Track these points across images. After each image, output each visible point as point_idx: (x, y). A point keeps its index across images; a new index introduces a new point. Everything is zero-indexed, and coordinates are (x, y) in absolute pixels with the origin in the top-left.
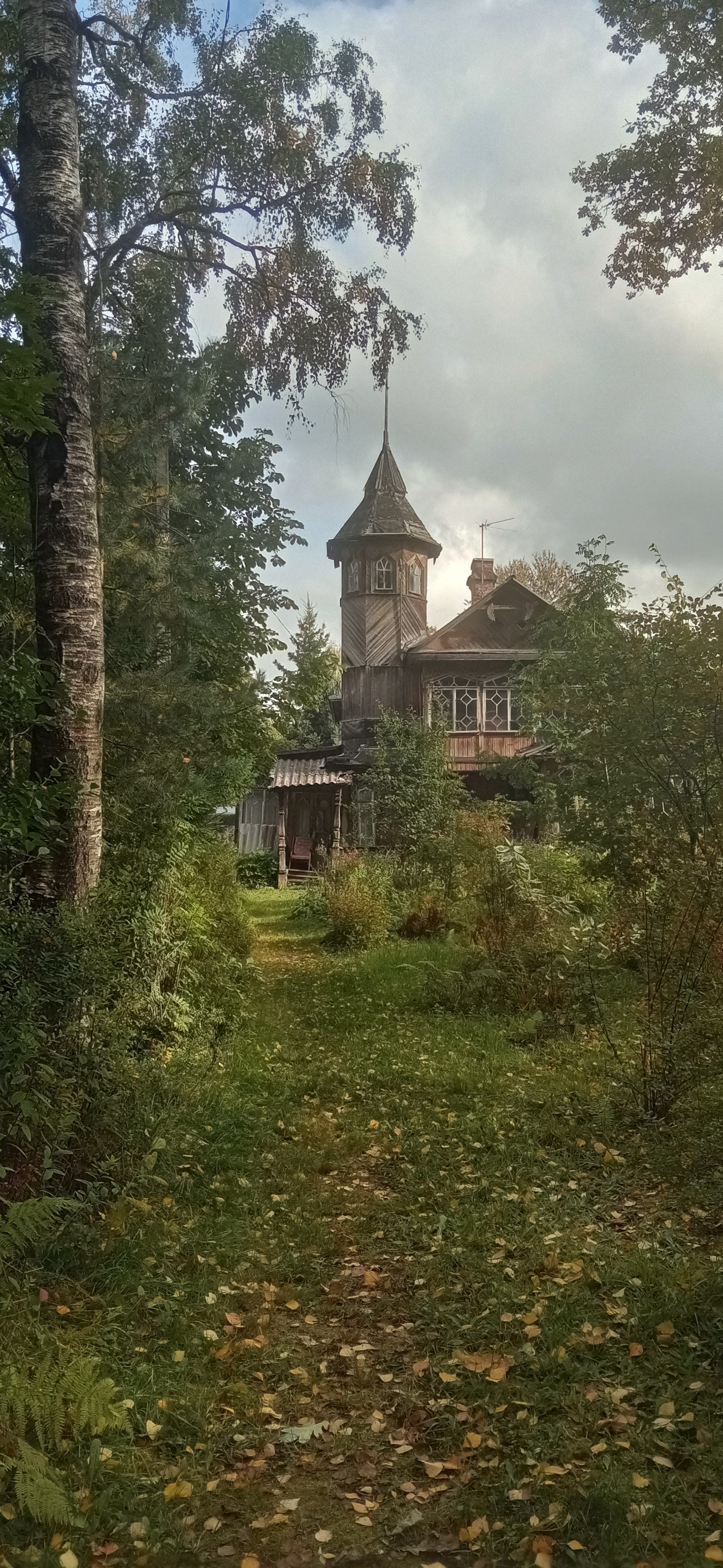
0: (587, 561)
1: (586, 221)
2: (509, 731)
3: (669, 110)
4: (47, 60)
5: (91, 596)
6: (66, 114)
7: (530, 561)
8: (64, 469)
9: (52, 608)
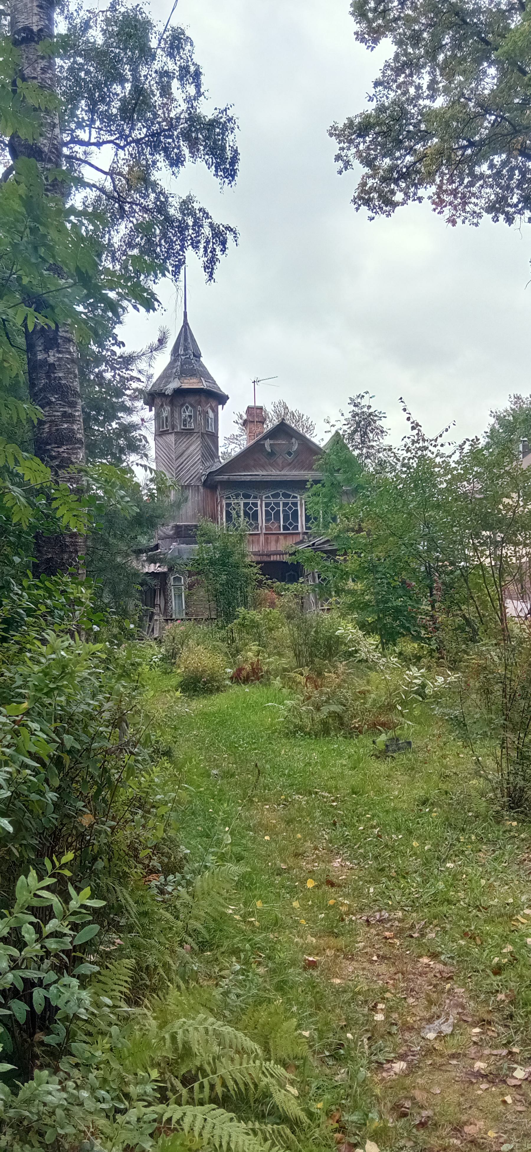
0: (356, 409)
1: (341, 164)
2: (282, 531)
3: (394, 86)
4: (35, 29)
5: (78, 436)
6: (50, 71)
7: (269, 409)
8: (57, 340)
9: (50, 444)
